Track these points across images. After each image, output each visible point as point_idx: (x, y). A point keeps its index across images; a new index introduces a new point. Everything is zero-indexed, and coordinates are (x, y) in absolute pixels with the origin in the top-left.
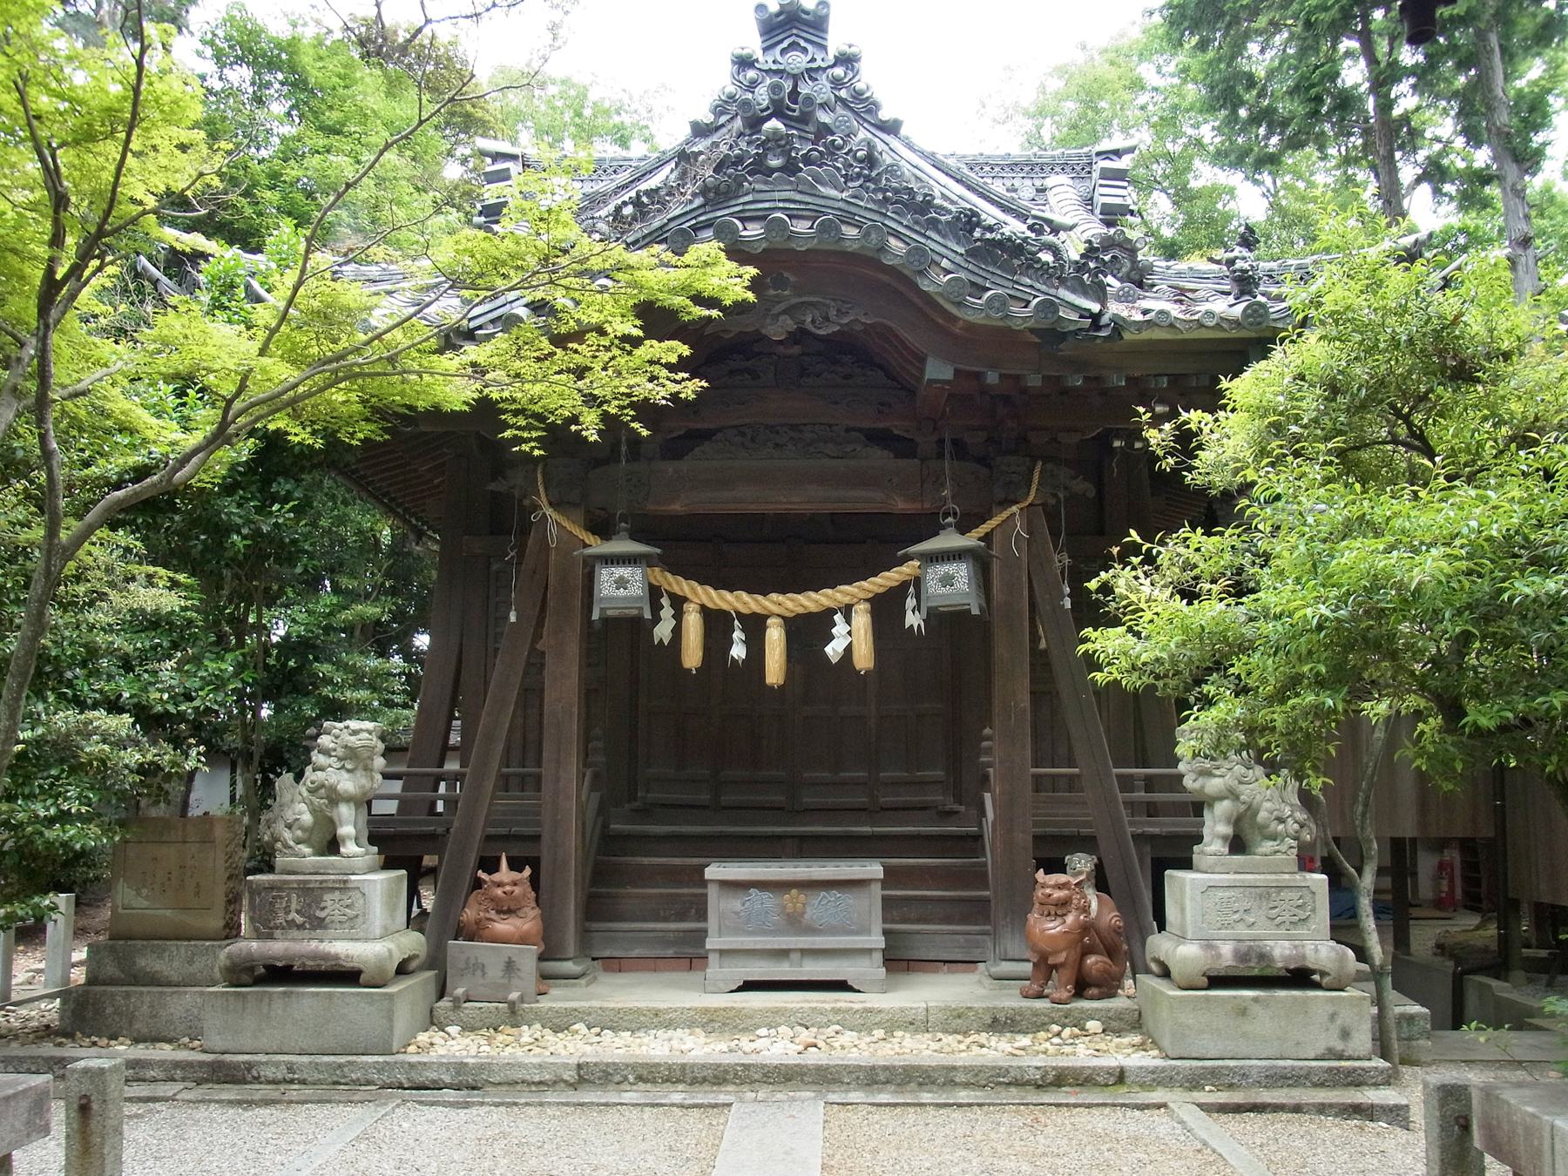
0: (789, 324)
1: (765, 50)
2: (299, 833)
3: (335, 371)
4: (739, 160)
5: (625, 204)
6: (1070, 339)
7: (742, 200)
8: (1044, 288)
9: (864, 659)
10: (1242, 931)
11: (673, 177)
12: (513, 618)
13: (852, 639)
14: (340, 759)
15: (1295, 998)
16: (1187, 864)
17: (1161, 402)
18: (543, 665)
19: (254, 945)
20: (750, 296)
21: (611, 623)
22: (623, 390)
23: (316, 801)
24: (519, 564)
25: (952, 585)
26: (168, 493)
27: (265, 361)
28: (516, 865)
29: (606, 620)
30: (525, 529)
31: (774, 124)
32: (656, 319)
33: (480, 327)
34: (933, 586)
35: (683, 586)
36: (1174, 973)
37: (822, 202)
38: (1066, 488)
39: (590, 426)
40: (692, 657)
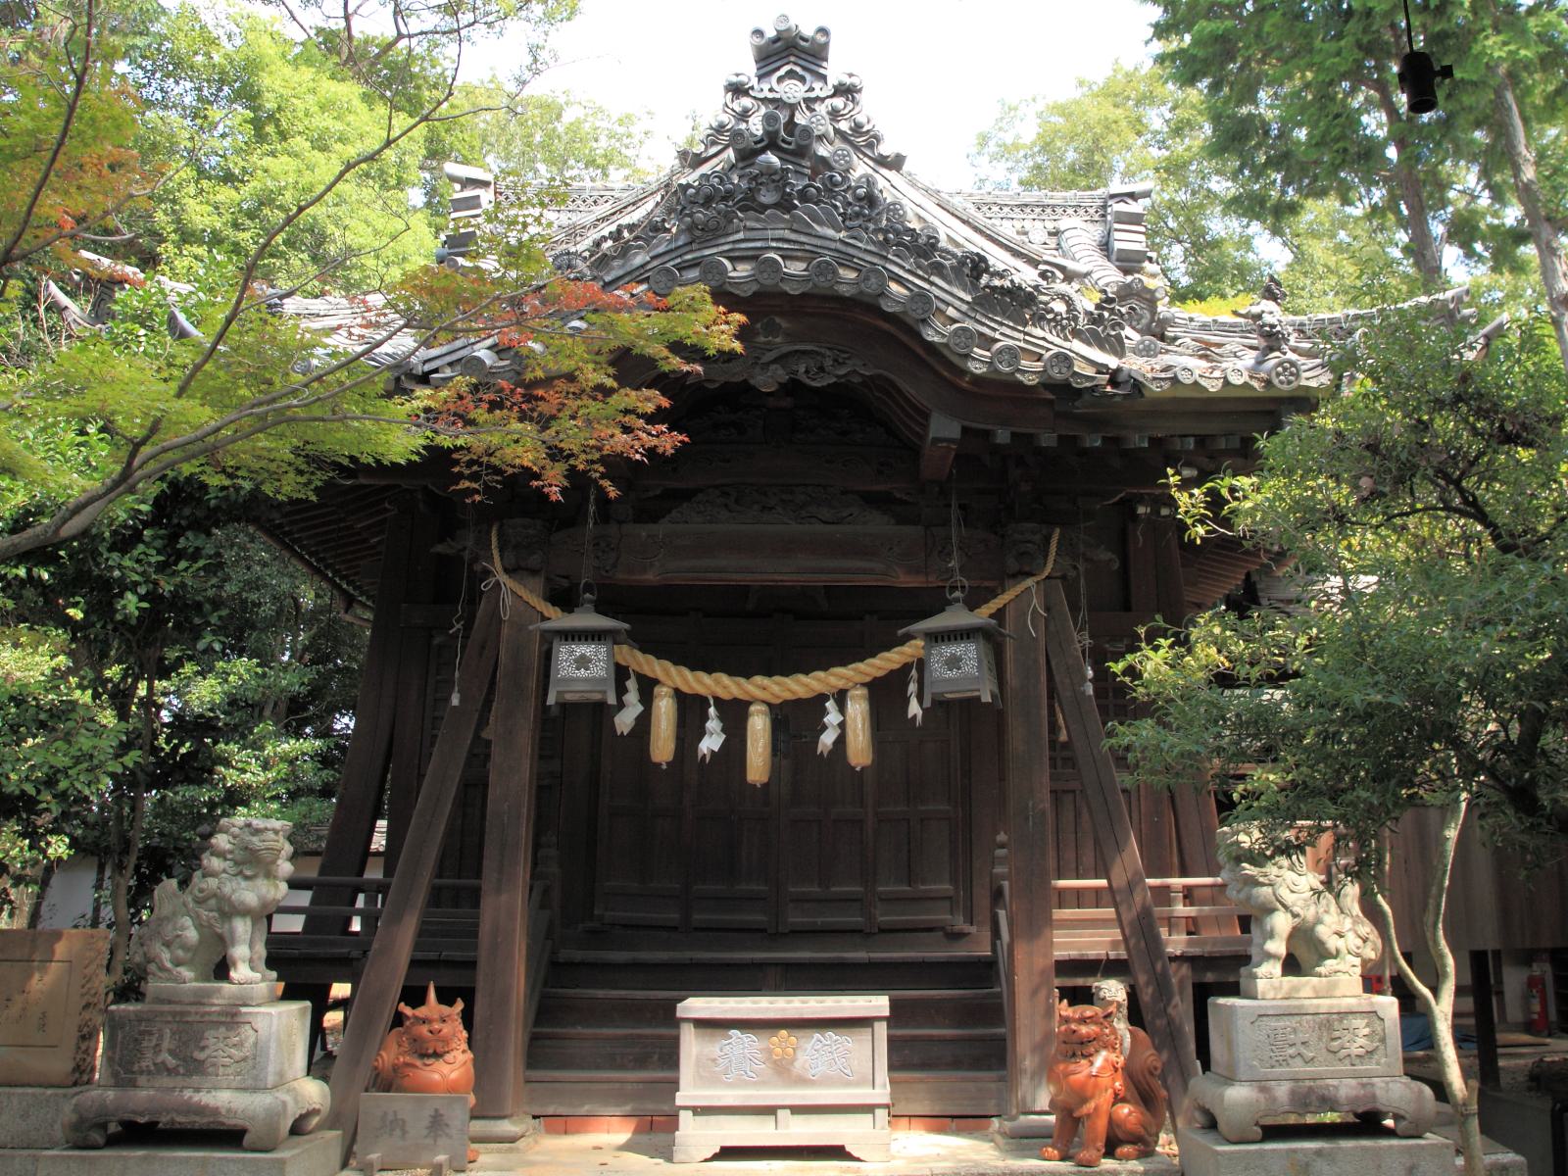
0: (781, 374)
1: (760, 77)
2: (180, 953)
3: (262, 417)
4: (728, 196)
5: (604, 239)
6: (1086, 397)
7: (731, 239)
8: (1057, 341)
9: (860, 750)
10: (1298, 1068)
11: (657, 211)
12: (455, 701)
13: (850, 727)
14: (237, 863)
15: (1364, 1149)
16: (1234, 990)
17: (1188, 464)
18: (488, 756)
19: (111, 1094)
20: (737, 346)
21: (569, 709)
22: (592, 442)
23: (204, 914)
24: (466, 637)
25: (960, 669)
26: (53, 545)
27: (183, 402)
28: (446, 997)
29: (565, 707)
30: (475, 597)
31: (772, 158)
32: (630, 366)
33: (436, 371)
34: (938, 669)
35: (654, 666)
36: (1221, 1125)
37: (819, 242)
38: (1087, 560)
39: (554, 483)
40: (663, 746)
